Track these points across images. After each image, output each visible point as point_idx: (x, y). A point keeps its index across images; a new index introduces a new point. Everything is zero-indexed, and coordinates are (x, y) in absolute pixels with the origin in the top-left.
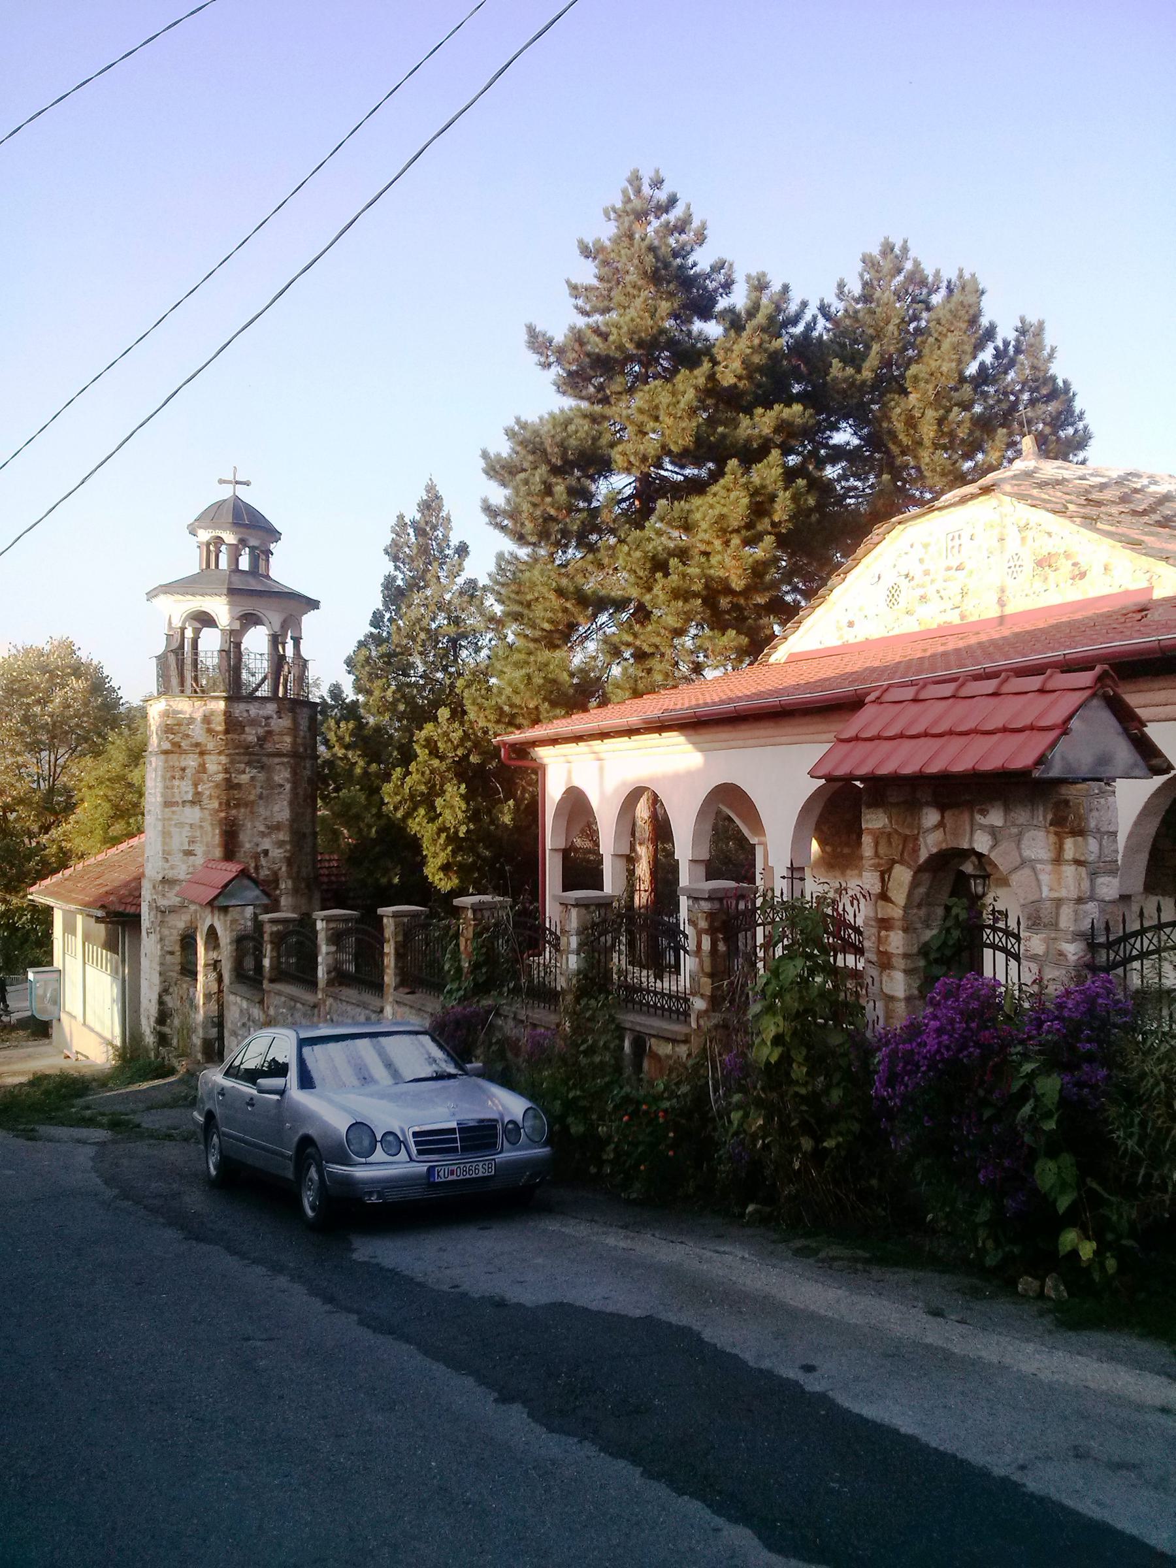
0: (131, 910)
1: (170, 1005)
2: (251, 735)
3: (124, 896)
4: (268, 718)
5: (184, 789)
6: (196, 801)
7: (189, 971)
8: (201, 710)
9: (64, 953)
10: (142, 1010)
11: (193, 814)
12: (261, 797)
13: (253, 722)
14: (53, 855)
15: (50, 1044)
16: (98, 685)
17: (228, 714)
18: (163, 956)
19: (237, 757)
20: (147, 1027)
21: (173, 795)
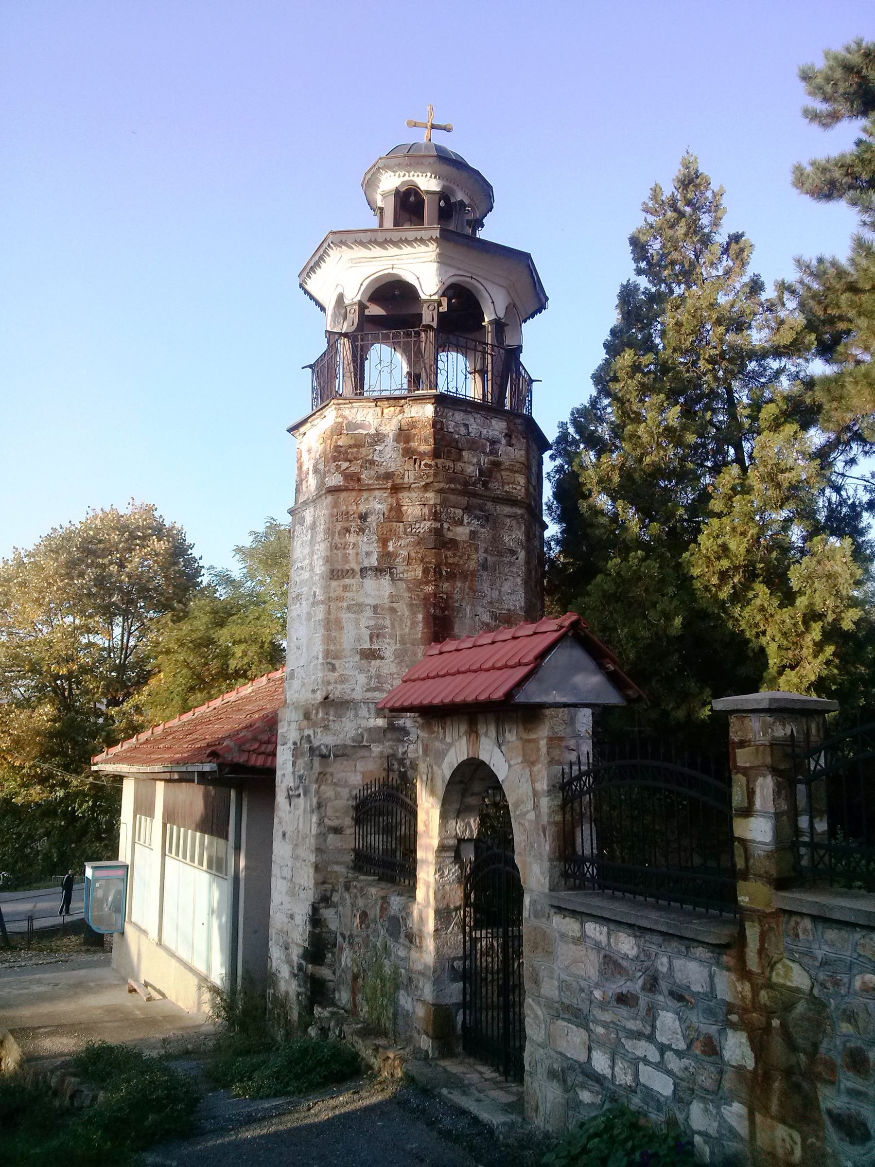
0: (258, 761)
1: (333, 926)
2: (471, 465)
4: (494, 442)
5: (365, 548)
6: (385, 567)
7: (395, 866)
8: (395, 421)
9: (134, 843)
10: (272, 932)
11: (378, 590)
12: (484, 566)
13: (474, 445)
14: (122, 731)
15: (107, 963)
16: (179, 550)
17: (437, 425)
18: (321, 836)
19: (452, 497)
20: (283, 964)
21: (346, 560)
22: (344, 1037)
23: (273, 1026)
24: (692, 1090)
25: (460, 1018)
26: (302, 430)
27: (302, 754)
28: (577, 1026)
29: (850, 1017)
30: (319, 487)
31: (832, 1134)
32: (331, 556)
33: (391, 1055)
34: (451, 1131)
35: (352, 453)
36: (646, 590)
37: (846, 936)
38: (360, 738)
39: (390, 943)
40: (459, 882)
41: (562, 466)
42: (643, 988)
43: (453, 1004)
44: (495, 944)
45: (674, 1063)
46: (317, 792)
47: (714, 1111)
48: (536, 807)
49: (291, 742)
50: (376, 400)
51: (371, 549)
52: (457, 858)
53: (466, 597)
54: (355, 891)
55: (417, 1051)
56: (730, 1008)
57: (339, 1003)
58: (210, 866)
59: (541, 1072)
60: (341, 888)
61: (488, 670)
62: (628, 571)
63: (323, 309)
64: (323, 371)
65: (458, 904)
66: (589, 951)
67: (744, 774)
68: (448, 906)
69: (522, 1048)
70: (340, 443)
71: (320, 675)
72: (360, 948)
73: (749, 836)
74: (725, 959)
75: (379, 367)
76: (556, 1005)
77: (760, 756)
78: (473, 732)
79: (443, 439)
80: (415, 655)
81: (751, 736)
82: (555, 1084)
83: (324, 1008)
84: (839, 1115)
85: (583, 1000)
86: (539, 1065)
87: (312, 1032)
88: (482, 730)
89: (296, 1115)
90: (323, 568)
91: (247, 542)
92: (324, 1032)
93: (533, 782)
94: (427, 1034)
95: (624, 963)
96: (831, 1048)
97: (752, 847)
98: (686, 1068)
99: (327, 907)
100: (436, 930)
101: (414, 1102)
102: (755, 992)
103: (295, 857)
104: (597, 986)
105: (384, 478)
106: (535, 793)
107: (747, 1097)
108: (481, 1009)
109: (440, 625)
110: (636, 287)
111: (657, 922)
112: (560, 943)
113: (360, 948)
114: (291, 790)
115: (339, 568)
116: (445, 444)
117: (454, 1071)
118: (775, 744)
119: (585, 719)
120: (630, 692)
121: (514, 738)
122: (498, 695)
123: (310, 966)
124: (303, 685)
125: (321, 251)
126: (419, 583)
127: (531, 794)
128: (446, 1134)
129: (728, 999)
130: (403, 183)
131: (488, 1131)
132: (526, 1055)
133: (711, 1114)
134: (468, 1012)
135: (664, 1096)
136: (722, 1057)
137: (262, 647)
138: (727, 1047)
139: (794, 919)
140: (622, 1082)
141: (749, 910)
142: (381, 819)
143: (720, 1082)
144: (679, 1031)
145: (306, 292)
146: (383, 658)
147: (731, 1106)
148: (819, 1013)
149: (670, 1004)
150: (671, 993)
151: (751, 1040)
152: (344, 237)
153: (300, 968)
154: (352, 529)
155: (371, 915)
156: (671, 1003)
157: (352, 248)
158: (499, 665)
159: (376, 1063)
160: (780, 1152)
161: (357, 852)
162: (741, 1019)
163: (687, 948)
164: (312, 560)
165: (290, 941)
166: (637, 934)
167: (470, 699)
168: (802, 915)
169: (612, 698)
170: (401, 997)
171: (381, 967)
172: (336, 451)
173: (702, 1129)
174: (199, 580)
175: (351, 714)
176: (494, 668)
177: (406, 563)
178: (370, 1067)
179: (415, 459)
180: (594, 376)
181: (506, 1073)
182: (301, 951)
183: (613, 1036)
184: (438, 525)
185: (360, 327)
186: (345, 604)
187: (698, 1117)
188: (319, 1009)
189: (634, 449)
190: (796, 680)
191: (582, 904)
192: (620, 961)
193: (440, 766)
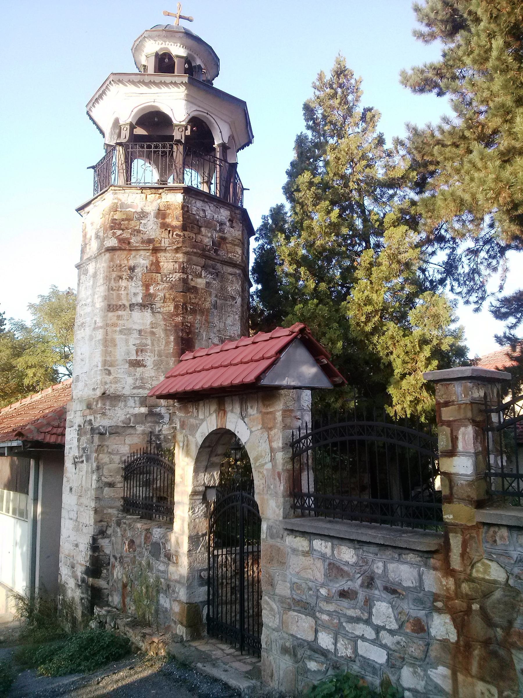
0: (52, 439)
1: (108, 551)
2: (207, 237)
3: (42, 425)
4: (222, 224)
5: (133, 290)
6: (148, 304)
7: (157, 506)
10: (62, 556)
11: (142, 319)
12: (215, 306)
13: (209, 225)
17: (185, 208)
18: (100, 489)
19: (194, 258)
20: (70, 579)
21: (119, 297)
22: (118, 628)
23: (62, 621)
24: (403, 659)
25: (205, 612)
26: (87, 209)
27: (85, 433)
28: (306, 615)
30: (99, 249)
32: (108, 295)
33: (156, 640)
34: (209, 694)
35: (124, 225)
36: (319, 325)
38: (128, 421)
39: (153, 561)
40: (206, 517)
41: (263, 245)
42: (362, 586)
43: (201, 602)
44: (229, 558)
45: (387, 639)
46: (97, 459)
49: (77, 425)
50: (142, 188)
51: (137, 291)
52: (205, 500)
53: (203, 326)
54: (125, 526)
55: (175, 636)
56: (436, 597)
57: (112, 604)
58: (14, 513)
60: (113, 524)
61: (236, 364)
62: (308, 313)
63: (102, 132)
64: (102, 173)
65: (204, 532)
66: (316, 560)
67: (449, 426)
68: (198, 533)
69: (259, 632)
70: (115, 217)
71: (99, 378)
72: (128, 566)
73: (453, 470)
75: (143, 166)
76: (289, 600)
77: (462, 411)
78: (221, 409)
79: (189, 217)
80: (168, 364)
81: (454, 398)
82: (287, 657)
83: (101, 607)
85: (310, 596)
86: (274, 644)
87: (93, 624)
88: (228, 408)
89: (89, 688)
90: (102, 304)
91: (37, 301)
92: (102, 624)
94: (182, 624)
95: (346, 568)
98: (398, 643)
99: (103, 538)
100: (189, 551)
101: (177, 674)
102: (458, 585)
103: (79, 505)
104: (323, 585)
105: (147, 243)
106: (272, 450)
107: (451, 662)
109: (186, 343)
110: (306, 137)
111: (375, 537)
112: (292, 556)
113: (128, 566)
114: (76, 458)
115: (114, 303)
116: (190, 223)
117: (203, 649)
118: (474, 403)
119: (307, 396)
120: (336, 379)
121: (255, 412)
122: (251, 378)
123: (91, 579)
124: (86, 385)
125: (104, 87)
126: (172, 315)
127: (268, 450)
129: (434, 591)
130: (161, 49)
132: (263, 637)
133: (419, 675)
134: (211, 606)
135: (379, 664)
136: (429, 634)
137: (46, 371)
138: (433, 626)
139: (492, 529)
140: (343, 655)
142: (141, 477)
143: (427, 652)
144: (392, 615)
145: (91, 118)
146: (145, 366)
147: (437, 669)
148: (514, 598)
149: (384, 596)
150: (386, 589)
151: (454, 620)
152: (121, 77)
153: (83, 581)
154: (124, 277)
155: (137, 542)
156: (384, 595)
157: (126, 86)
158: (246, 360)
159: (144, 646)
161: (125, 499)
162: (446, 605)
164: (93, 299)
165: (75, 562)
166: (357, 546)
167: (226, 383)
169: (325, 383)
170: (161, 599)
171: (146, 578)
172: (112, 223)
173: (412, 687)
174: (3, 327)
175: (121, 404)
176: (241, 363)
177: (162, 301)
178: (139, 649)
180: (284, 188)
181: (241, 649)
182: (84, 569)
184: (185, 276)
185: (130, 140)
186: (118, 329)
187: (408, 678)
188: (98, 609)
189: (309, 236)
190: (414, 382)
192: (342, 567)
193: (193, 435)
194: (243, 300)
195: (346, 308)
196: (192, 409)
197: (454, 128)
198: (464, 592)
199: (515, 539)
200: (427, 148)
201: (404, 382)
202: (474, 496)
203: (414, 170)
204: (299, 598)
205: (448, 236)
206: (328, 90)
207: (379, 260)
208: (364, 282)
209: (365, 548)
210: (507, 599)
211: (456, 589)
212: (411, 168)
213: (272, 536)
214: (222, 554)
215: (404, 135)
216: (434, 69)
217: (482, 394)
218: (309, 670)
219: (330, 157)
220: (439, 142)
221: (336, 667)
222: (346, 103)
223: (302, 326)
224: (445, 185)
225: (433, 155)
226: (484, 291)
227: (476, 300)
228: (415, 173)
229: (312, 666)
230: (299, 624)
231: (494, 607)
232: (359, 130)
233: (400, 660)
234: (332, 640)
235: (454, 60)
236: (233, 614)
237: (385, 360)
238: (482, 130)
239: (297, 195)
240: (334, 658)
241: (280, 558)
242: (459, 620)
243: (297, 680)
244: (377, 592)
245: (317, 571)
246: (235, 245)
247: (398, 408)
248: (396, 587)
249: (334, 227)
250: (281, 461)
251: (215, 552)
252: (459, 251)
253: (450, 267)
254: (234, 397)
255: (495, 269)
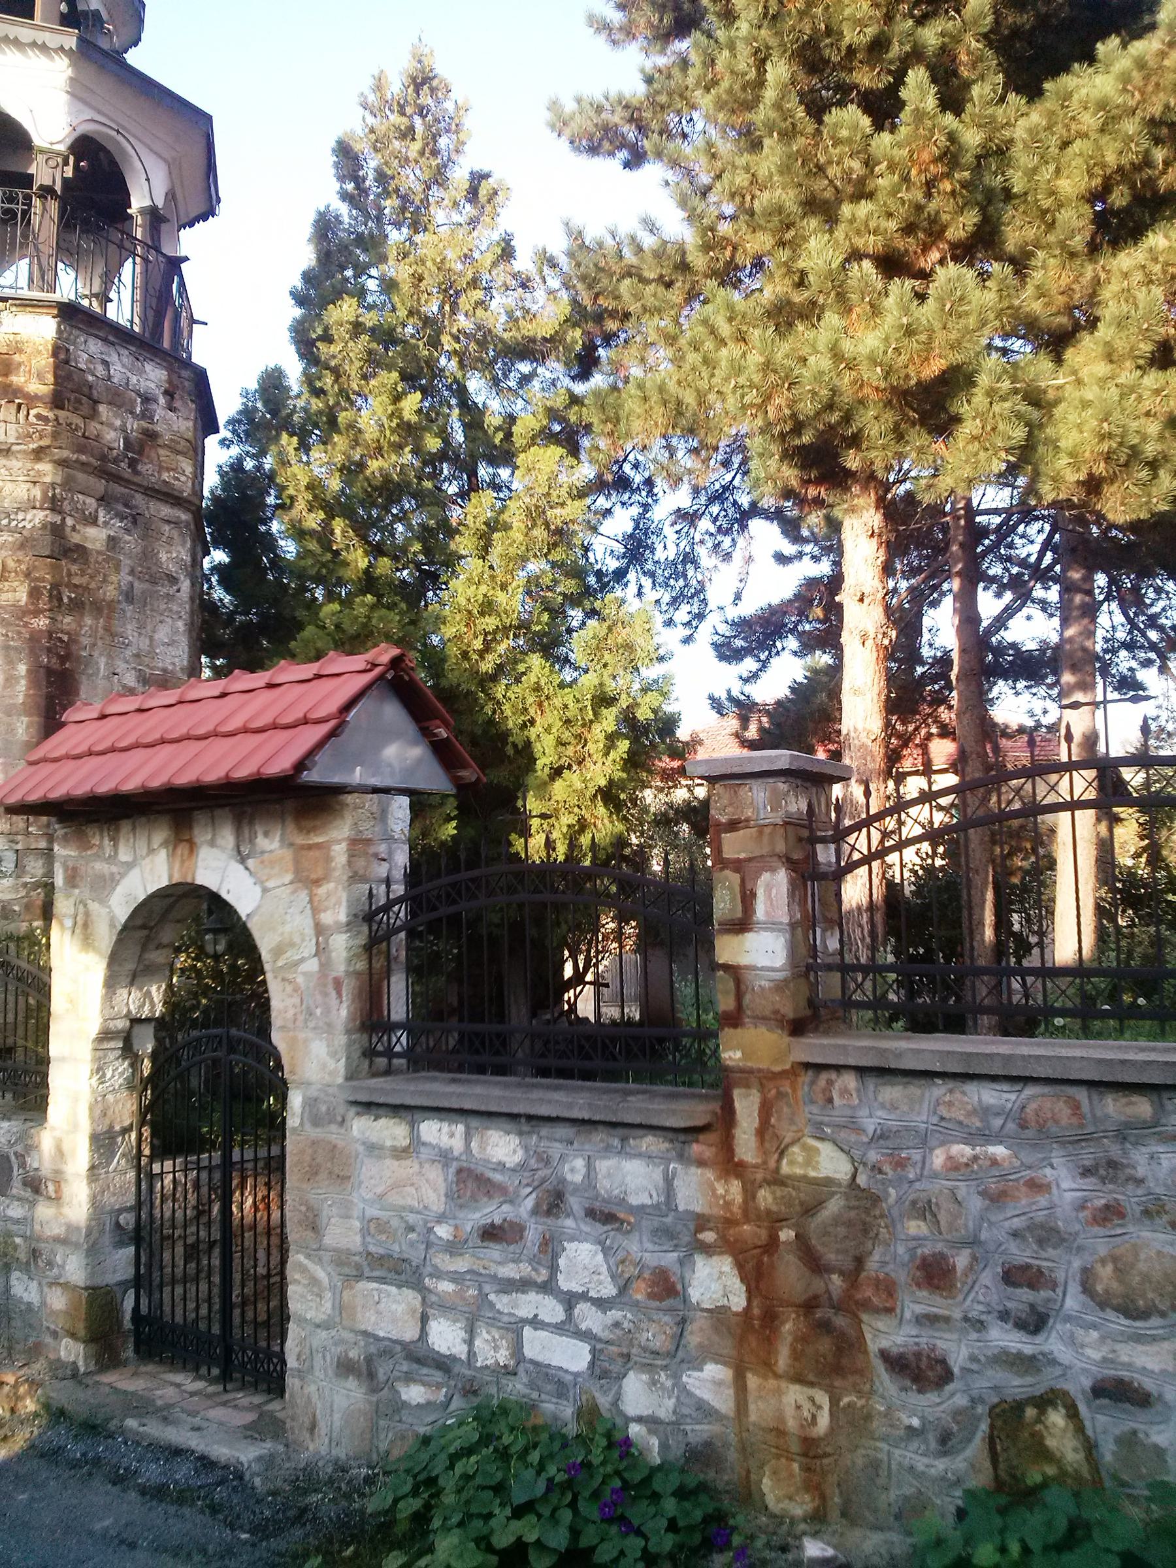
2: (112, 428)
4: (147, 399)
12: (129, 596)
13: (118, 398)
17: (61, 354)
19: (81, 476)
24: (627, 1357)
25: (129, 1303)
28: (399, 1287)
29: (925, 1210)
31: (886, 1382)
37: (918, 1092)
40: (131, 1087)
41: (240, 460)
42: (535, 1212)
43: (119, 1284)
45: (590, 1319)
47: (669, 1383)
48: (321, 951)
52: (128, 1050)
56: (701, 1222)
59: (322, 1369)
65: (127, 1123)
68: (111, 1127)
73: (744, 960)
74: (696, 1149)
77: (765, 839)
79: (69, 377)
82: (351, 1383)
84: (901, 1356)
85: (412, 1244)
86: (318, 1359)
93: (315, 911)
94: (73, 1335)
95: (497, 1177)
96: (889, 1258)
97: (749, 976)
98: (617, 1325)
100: (92, 1168)
101: (75, 1450)
102: (749, 1194)
104: (441, 1219)
106: (319, 929)
108: (161, 1287)
111: (570, 1106)
116: (71, 390)
122: (281, 765)
126: (23, 613)
127: (310, 931)
128: (157, 1493)
129: (698, 1209)
131: (234, 1475)
136: (686, 1300)
138: (694, 1283)
139: (824, 1076)
141: (742, 1071)
144: (604, 1269)
148: (867, 1211)
149: (586, 1228)
150: (591, 1213)
151: (740, 1266)
160: (791, 1424)
162: (723, 1237)
163: (624, 1140)
166: (526, 1128)
168: (838, 1068)
169: (434, 780)
179: (19, 406)
181: (225, 1378)
183: (472, 1292)
184: (57, 519)
187: (638, 1396)
190: (579, 785)
191: (421, 1093)
193: (103, 901)
194: (193, 585)
195: (438, 617)
196: (100, 840)
197: (665, 243)
198: (762, 1205)
199: (871, 1095)
200: (605, 281)
201: (558, 785)
202: (789, 1011)
203: (575, 325)
204: (381, 1251)
205: (638, 479)
206: (395, 118)
207: (505, 517)
208: (472, 565)
209: (545, 1131)
210: (853, 1214)
211: (745, 1202)
212: (570, 322)
213: (316, 1121)
214: (168, 1170)
215: (558, 246)
216: (627, 107)
217: (804, 807)
218: (405, 1404)
219: (400, 271)
220: (629, 272)
221: (470, 1391)
222: (435, 153)
223: (395, 651)
224: (646, 364)
225: (617, 298)
226: (704, 601)
227: (687, 618)
228: (578, 333)
229: (414, 1394)
230: (382, 1306)
231: (826, 1233)
232: (461, 220)
233: (620, 1361)
234: (463, 1334)
235: (670, 94)
236: (191, 1305)
237: (517, 738)
238: (733, 257)
239: (323, 348)
240: (468, 1372)
241: (336, 1168)
242: (750, 1266)
243: (374, 1430)
244: (569, 1223)
245: (429, 1189)
246: (179, 453)
247: (537, 841)
248: (614, 1209)
249: (409, 432)
250: (344, 954)
251: (156, 1168)
252: (661, 512)
253: (637, 547)
254: (218, 812)
255: (727, 557)
